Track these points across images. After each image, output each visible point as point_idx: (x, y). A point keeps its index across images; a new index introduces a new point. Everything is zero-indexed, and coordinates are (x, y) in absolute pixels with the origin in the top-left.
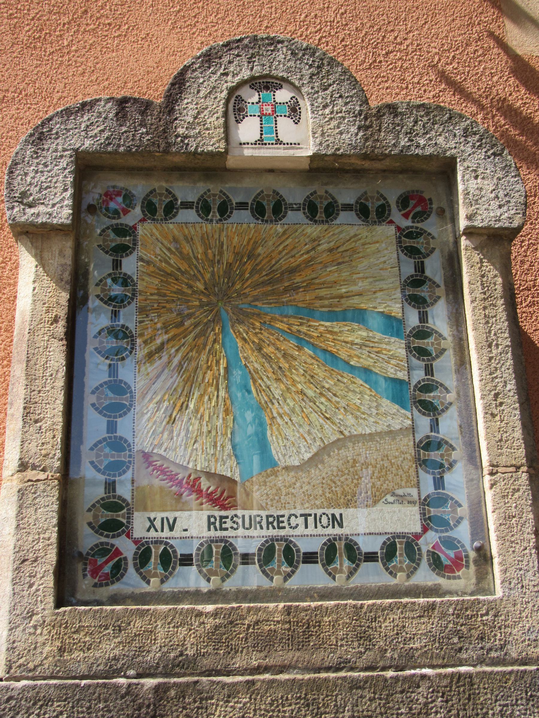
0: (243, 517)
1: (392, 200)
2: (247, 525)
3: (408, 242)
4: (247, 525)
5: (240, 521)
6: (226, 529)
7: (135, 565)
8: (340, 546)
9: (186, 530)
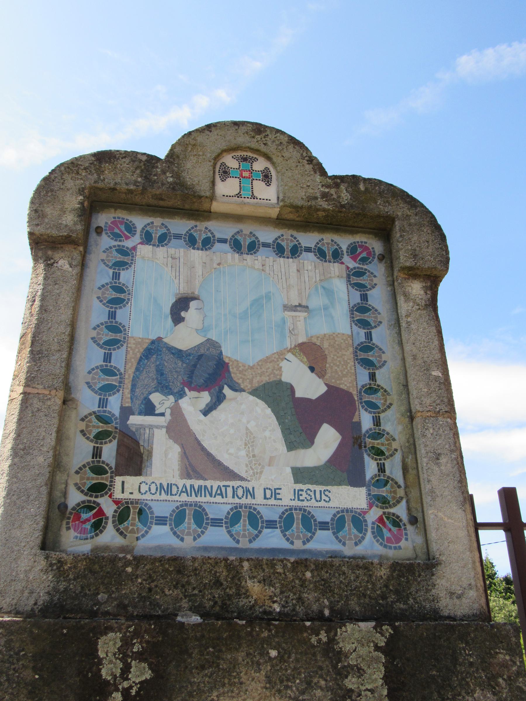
0: (315, 491)
1: (344, 248)
2: (318, 497)
3: (355, 280)
4: (318, 497)
5: (312, 494)
6: (303, 500)
7: (114, 522)
8: (297, 516)
9: (131, 493)
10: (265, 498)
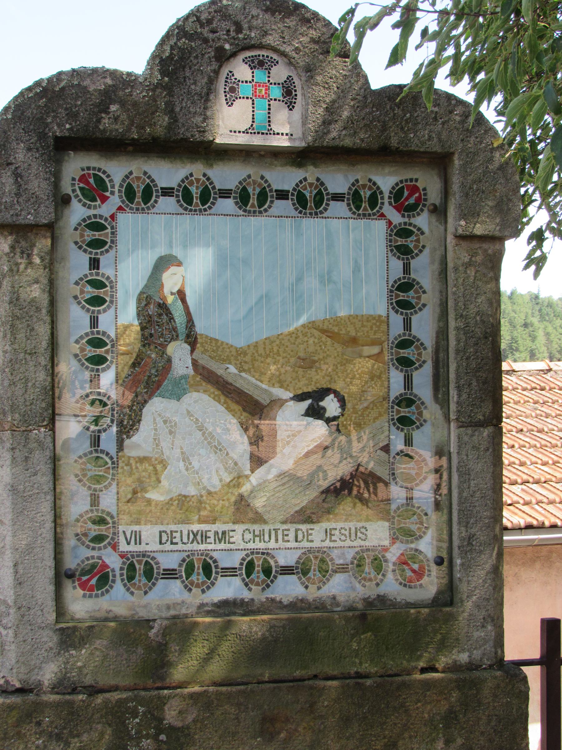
4: (185, 540)
9: (147, 544)
10: (161, 543)
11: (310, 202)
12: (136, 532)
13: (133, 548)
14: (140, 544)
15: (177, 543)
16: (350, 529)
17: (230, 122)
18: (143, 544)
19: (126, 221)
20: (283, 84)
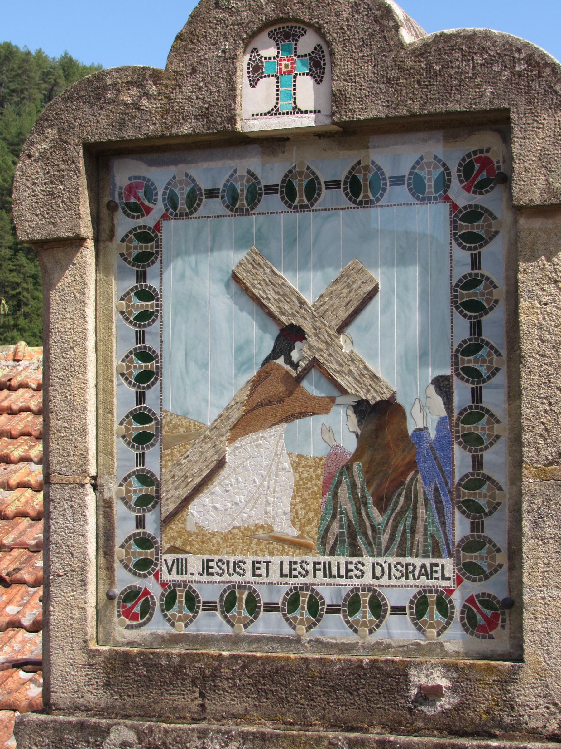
0: (228, 562)
2: (231, 571)
4: (231, 571)
5: (225, 567)
9: (192, 574)
11: (357, 189)
12: (182, 559)
13: (174, 577)
14: (186, 574)
15: (260, 575)
16: (324, 563)
17: (256, 107)
18: (189, 574)
19: (171, 228)
20: (310, 55)
